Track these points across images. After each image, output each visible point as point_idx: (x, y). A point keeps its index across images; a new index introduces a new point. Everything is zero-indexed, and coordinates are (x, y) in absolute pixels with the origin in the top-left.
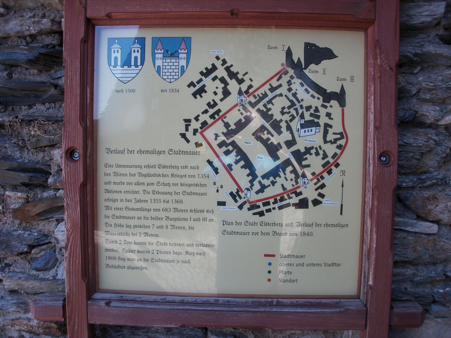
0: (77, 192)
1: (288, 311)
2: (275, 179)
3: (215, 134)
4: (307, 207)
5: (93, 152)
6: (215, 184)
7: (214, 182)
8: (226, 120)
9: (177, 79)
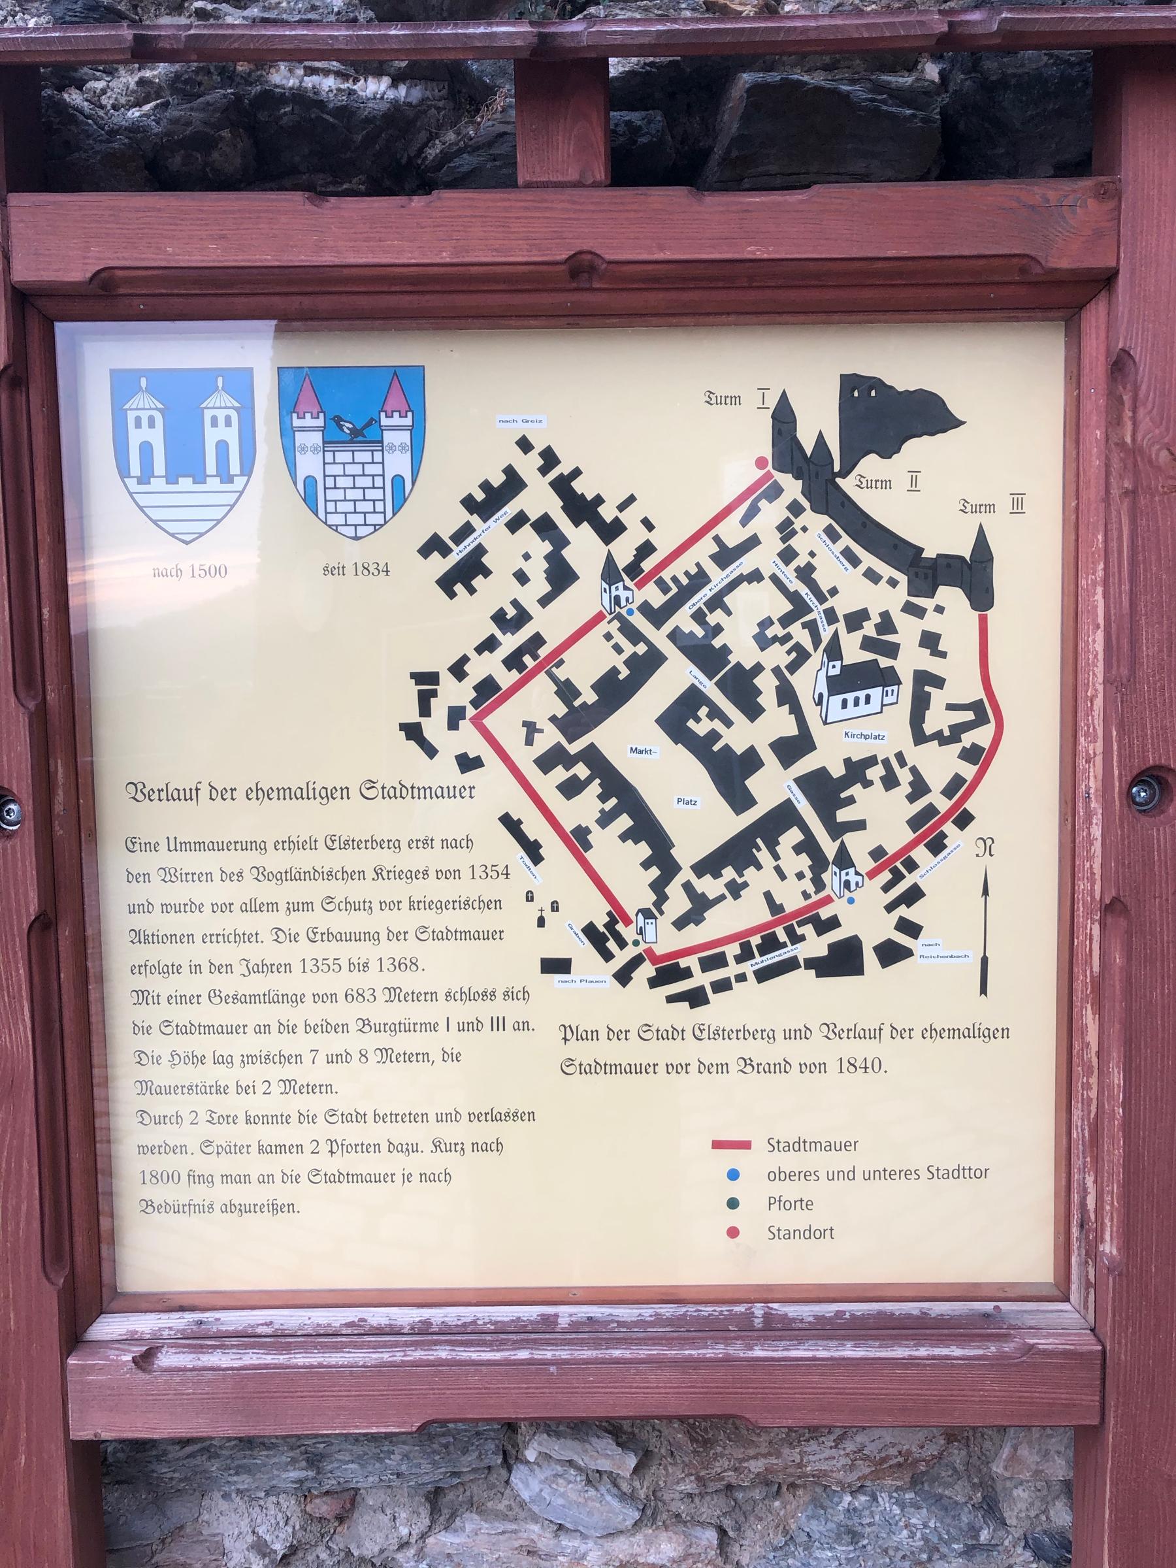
0: (15, 953)
1: (809, 1354)
2: (741, 875)
3: (526, 724)
4: (858, 970)
5: (78, 799)
6: (532, 898)
7: (527, 893)
8: (561, 674)
9: (382, 526)
